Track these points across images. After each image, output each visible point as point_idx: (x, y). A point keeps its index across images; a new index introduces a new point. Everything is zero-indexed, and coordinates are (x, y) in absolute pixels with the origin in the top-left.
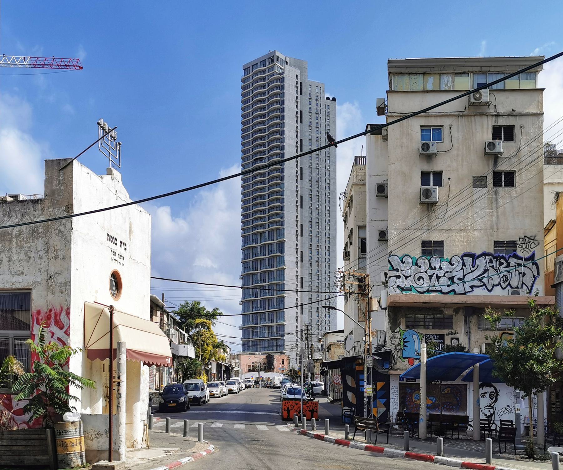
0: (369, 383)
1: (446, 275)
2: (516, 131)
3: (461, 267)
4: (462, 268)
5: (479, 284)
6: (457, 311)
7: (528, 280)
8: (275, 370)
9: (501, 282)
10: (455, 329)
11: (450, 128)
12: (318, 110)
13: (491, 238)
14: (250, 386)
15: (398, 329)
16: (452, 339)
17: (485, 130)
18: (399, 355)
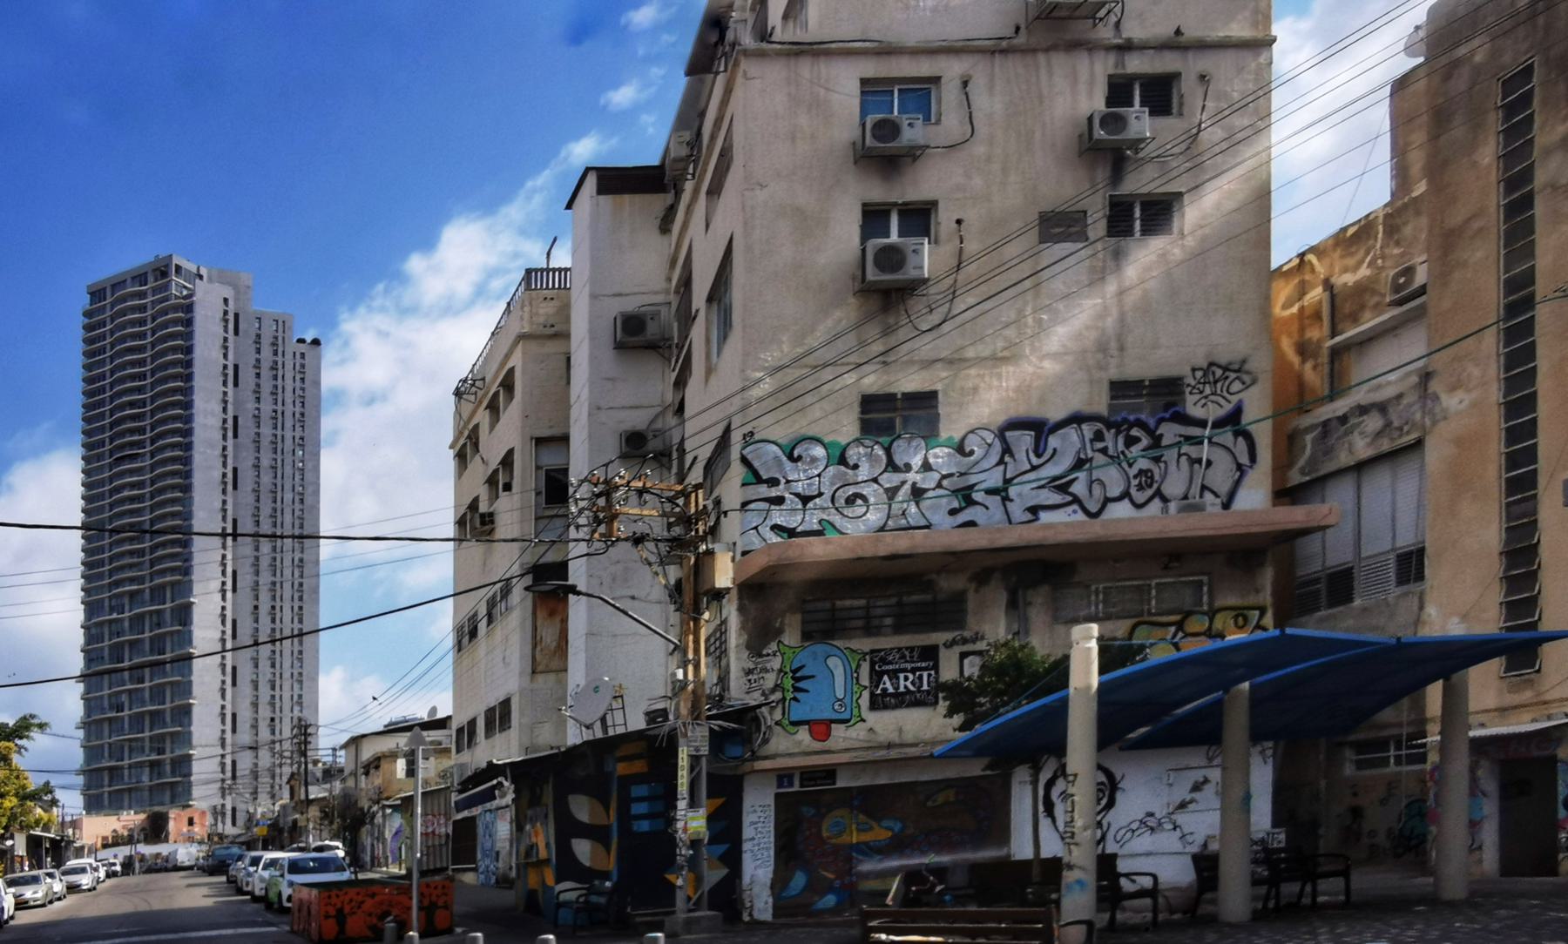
0: (693, 803)
1: (945, 483)
2: (1188, 86)
3: (994, 459)
4: (1001, 462)
5: (1056, 498)
6: (982, 578)
7: (1221, 477)
8: (171, 838)
9: (1133, 491)
10: (976, 628)
11: (965, 84)
12: (276, 363)
13: (1097, 375)
14: (115, 874)
15: (773, 646)
16: (963, 656)
17: (1082, 88)
18: (778, 715)
